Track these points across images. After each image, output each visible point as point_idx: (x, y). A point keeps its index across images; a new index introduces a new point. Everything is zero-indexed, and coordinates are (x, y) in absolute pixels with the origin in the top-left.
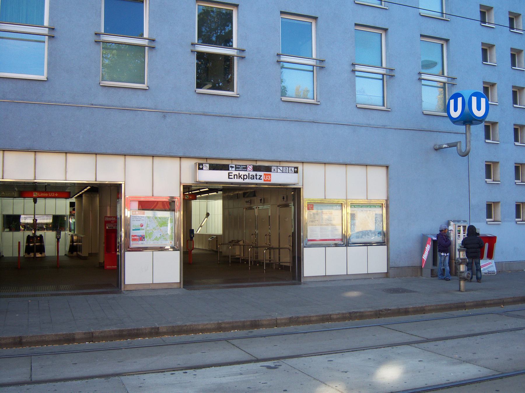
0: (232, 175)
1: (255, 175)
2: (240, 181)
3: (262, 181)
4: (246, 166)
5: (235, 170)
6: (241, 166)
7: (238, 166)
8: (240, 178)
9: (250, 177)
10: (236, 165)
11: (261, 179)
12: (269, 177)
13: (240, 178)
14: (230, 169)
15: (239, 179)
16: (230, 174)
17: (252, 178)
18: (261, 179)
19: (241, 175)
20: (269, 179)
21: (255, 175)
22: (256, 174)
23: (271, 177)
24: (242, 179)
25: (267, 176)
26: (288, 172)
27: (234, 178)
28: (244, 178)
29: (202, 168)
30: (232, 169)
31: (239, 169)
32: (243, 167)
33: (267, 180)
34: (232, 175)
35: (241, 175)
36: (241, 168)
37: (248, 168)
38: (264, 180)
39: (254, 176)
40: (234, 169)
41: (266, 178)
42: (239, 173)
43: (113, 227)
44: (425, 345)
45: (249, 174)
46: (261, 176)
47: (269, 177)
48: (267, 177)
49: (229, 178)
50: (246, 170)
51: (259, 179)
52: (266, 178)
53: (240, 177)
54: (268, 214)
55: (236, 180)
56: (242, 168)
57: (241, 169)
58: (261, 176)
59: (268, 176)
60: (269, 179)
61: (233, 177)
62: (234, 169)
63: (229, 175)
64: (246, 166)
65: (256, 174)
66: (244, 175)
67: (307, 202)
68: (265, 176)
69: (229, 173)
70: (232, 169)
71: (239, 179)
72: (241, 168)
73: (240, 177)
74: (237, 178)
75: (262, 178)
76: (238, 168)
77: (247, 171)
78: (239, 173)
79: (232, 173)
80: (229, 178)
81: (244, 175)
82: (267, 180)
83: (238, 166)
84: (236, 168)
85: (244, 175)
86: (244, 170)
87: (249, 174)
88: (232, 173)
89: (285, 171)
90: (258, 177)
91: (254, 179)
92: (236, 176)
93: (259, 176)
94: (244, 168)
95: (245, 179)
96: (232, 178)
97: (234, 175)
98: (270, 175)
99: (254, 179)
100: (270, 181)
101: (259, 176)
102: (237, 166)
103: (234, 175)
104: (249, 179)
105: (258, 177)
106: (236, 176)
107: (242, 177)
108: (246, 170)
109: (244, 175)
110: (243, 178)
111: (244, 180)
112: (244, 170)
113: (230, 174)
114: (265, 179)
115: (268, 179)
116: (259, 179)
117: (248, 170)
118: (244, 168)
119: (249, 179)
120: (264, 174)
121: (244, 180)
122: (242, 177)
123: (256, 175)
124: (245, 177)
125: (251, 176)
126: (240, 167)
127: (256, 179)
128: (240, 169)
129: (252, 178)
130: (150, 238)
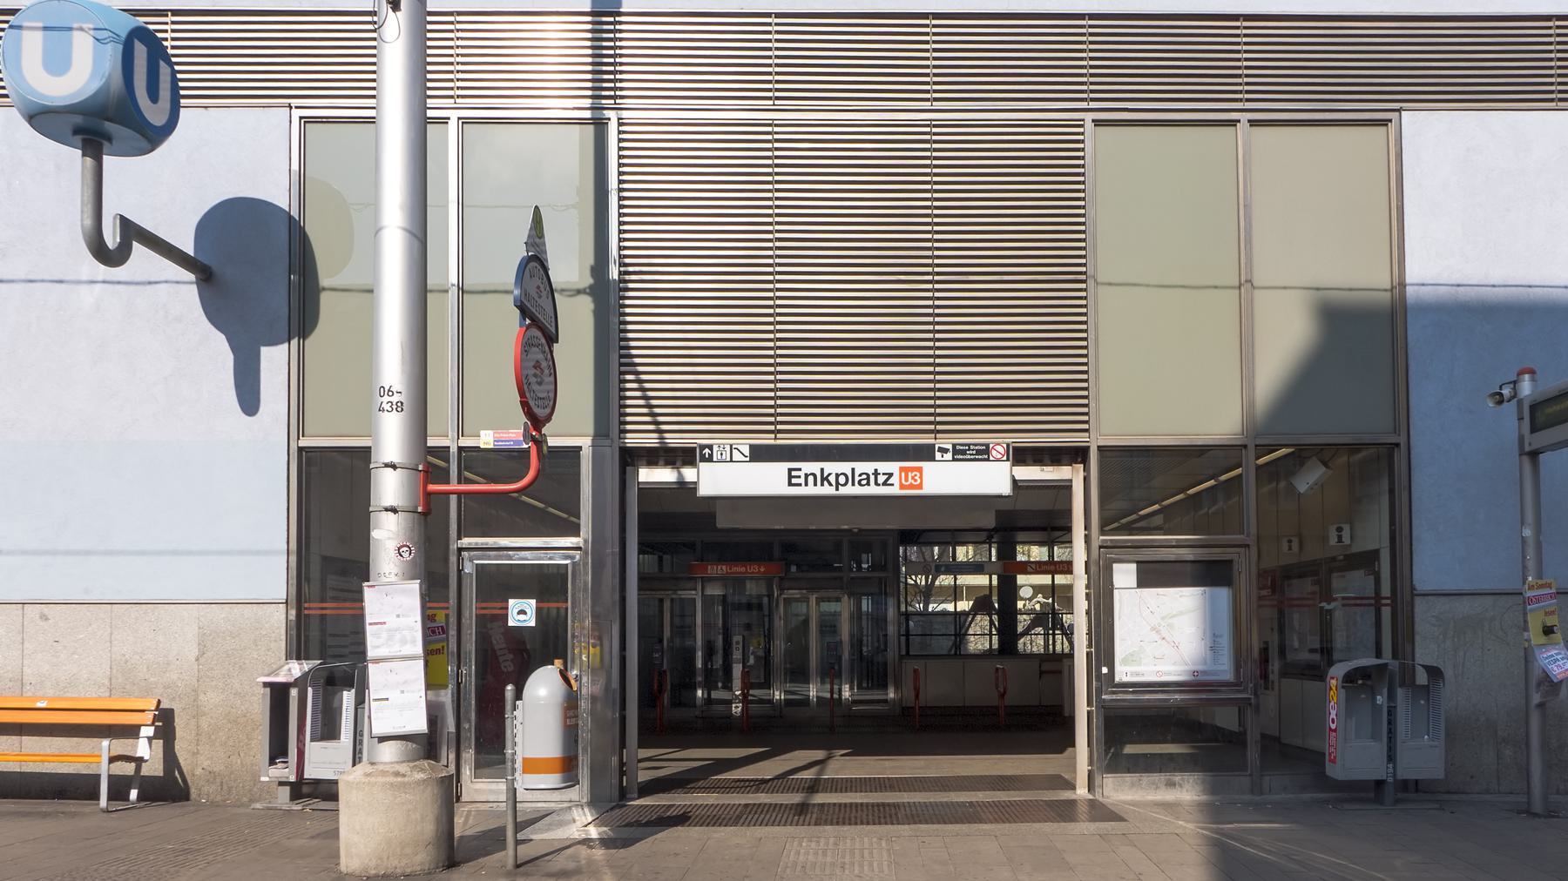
0: (799, 477)
1: (871, 471)
2: (827, 490)
3: (894, 490)
4: (987, 446)
5: (954, 460)
6: (972, 447)
7: (962, 448)
8: (825, 482)
9: (857, 479)
10: (954, 446)
11: (893, 485)
12: (916, 475)
13: (825, 482)
14: (938, 455)
15: (822, 485)
16: (794, 473)
17: (864, 482)
18: (893, 485)
19: (830, 474)
20: (916, 481)
21: (871, 471)
22: (876, 470)
23: (921, 477)
24: (830, 484)
25: (910, 473)
26: (728, 459)
27: (806, 484)
28: (838, 483)
29: (711, 455)
30: (942, 456)
31: (966, 454)
32: (977, 450)
33: (911, 487)
34: (799, 477)
35: (830, 474)
36: (971, 452)
37: (994, 452)
38: (902, 487)
39: (868, 479)
40: (949, 456)
41: (907, 480)
42: (822, 470)
43: (288, 778)
44: (569, 843)
45: (853, 470)
46: (890, 475)
47: (916, 475)
48: (910, 478)
49: (790, 484)
50: (986, 457)
51: (885, 484)
52: (907, 480)
53: (825, 479)
54: (1524, 448)
55: (811, 490)
56: (974, 452)
57: (973, 454)
58: (890, 475)
59: (913, 475)
60: (916, 481)
61: (802, 480)
62: (949, 456)
63: (790, 477)
64: (987, 446)
65: (876, 470)
66: (837, 476)
67: (1235, 557)
68: (903, 474)
69: (790, 470)
70: (942, 456)
71: (822, 485)
72: (971, 452)
73: (825, 479)
74: (815, 484)
75: (894, 480)
76: (963, 452)
77: (988, 460)
78: (822, 470)
79: (800, 470)
80: (790, 484)
81: (837, 476)
82: (911, 487)
83: (962, 448)
84: (955, 452)
85: (837, 474)
86: (980, 457)
87: (853, 470)
88: (800, 470)
89: (719, 457)
90: (881, 479)
91: (868, 484)
92: (811, 479)
93: (883, 474)
94: (979, 452)
95: (842, 485)
96: (800, 485)
97: (807, 476)
98: (920, 470)
99: (868, 484)
100: (920, 487)
101: (883, 474)
102: (958, 447)
103: (807, 476)
104: (853, 484)
105: (881, 479)
106: (811, 479)
107: (832, 479)
108: (986, 457)
109: (837, 474)
110: (833, 482)
111: (837, 489)
112: (980, 457)
113: (794, 473)
114: (903, 482)
115: (913, 482)
116: (885, 484)
117: (991, 458)
118: (979, 452)
119: (853, 484)
120: (902, 469)
121: (837, 489)
122: (832, 479)
123: (876, 473)
124: (842, 480)
125: (860, 475)
126: (969, 450)
127: (877, 484)
128: (969, 457)
129: (864, 482)
130: (232, 773)
